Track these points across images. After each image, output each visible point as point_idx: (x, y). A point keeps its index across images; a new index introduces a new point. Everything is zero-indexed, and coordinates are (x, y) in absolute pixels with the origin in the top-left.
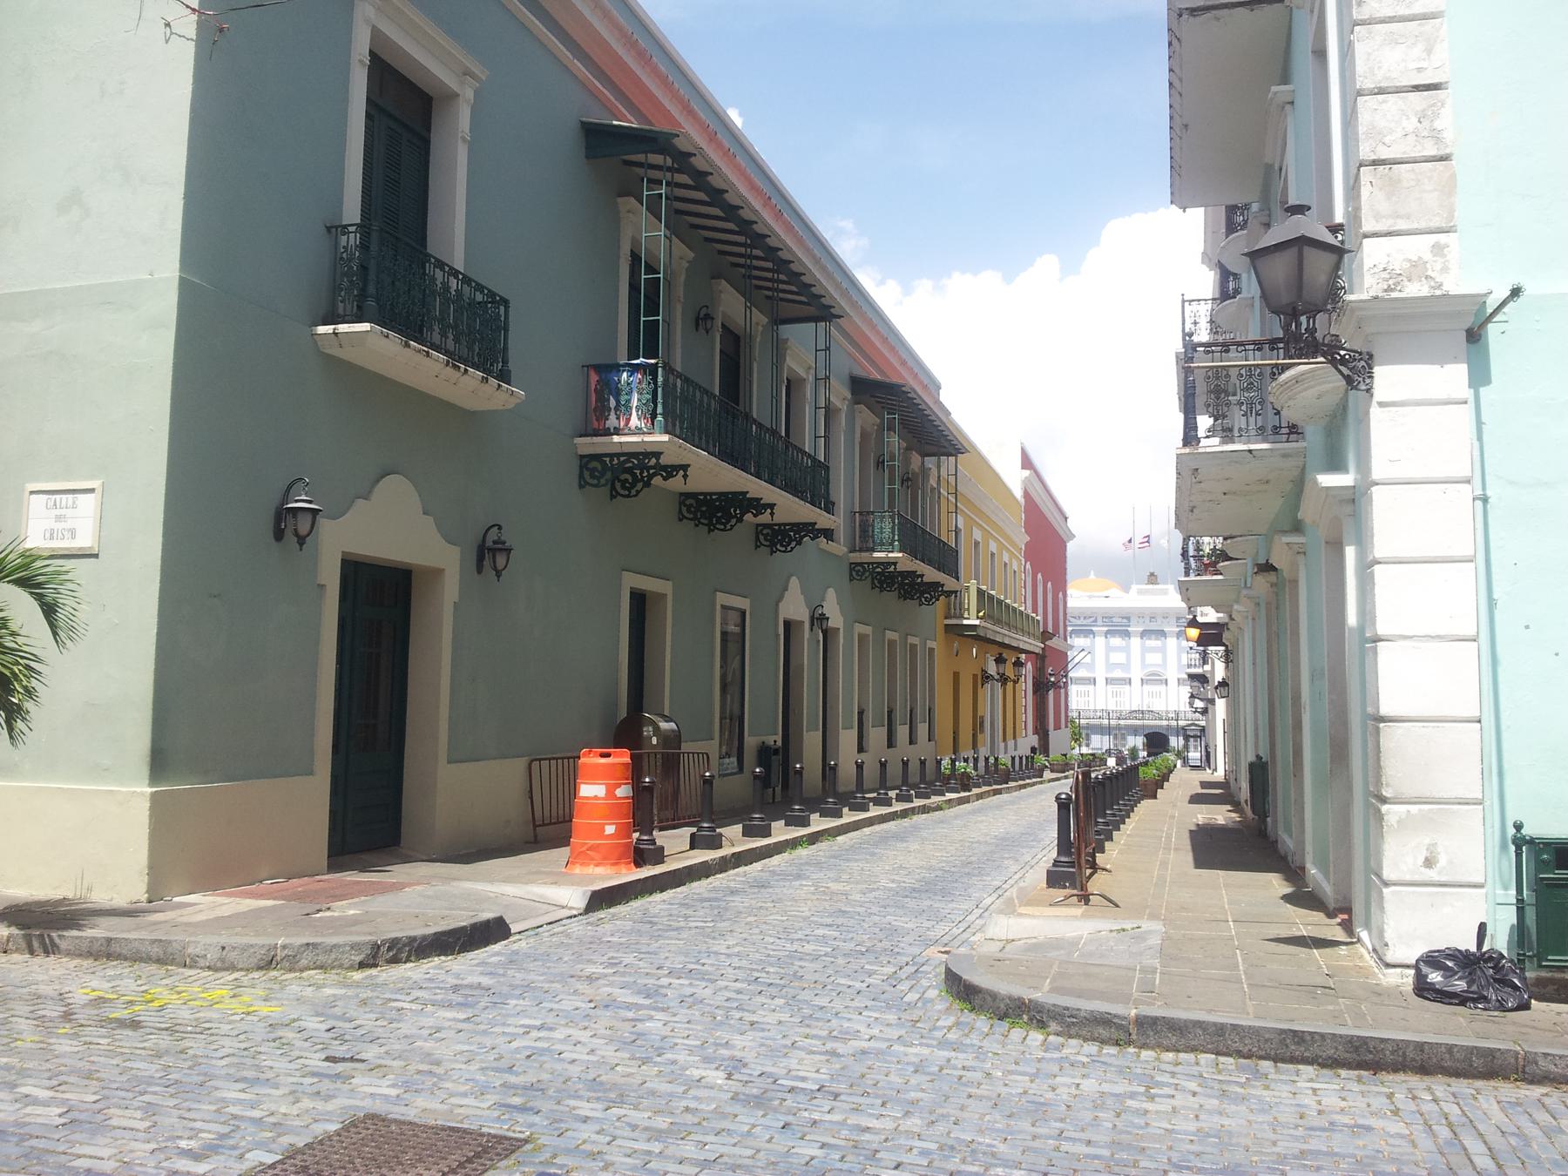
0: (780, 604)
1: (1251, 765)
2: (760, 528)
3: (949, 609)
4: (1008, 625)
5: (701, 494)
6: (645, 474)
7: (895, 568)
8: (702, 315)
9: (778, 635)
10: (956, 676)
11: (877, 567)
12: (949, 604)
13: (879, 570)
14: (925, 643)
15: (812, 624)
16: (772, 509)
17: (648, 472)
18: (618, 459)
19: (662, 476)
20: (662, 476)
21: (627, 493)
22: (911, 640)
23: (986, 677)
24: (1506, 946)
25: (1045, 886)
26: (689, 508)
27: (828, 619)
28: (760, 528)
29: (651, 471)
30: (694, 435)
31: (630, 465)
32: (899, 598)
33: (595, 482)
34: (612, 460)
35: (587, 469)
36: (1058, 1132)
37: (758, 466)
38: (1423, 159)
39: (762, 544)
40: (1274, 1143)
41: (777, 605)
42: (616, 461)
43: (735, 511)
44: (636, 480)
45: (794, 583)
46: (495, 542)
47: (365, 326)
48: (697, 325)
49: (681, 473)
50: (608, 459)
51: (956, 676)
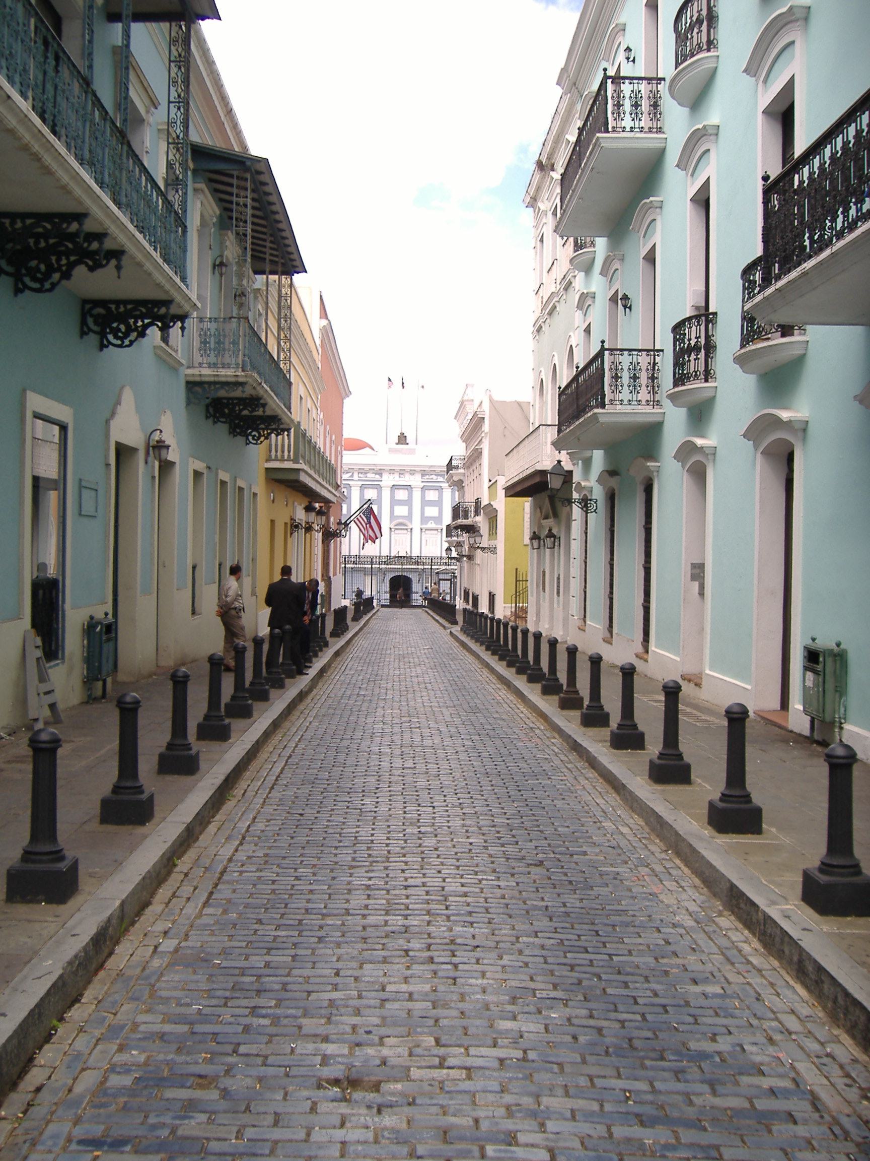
0: (111, 422)
2: (88, 306)
3: (270, 451)
4: (314, 467)
6: (64, 262)
7: (264, 411)
10: (272, 522)
12: (270, 445)
13: (245, 412)
14: (235, 481)
15: (147, 453)
16: (119, 260)
17: (68, 259)
18: (125, 307)
19: (87, 265)
20: (158, 326)
21: (119, 342)
22: (241, 483)
26: (96, 318)
27: (168, 447)
28: (88, 306)
29: (146, 321)
30: (84, 127)
31: (63, 248)
32: (207, 417)
33: (119, 342)
35: (91, 316)
38: (584, 535)
39: (90, 330)
41: (107, 422)
43: (59, 260)
44: (50, 270)
45: (128, 397)
46: (157, 442)
49: (179, 324)
50: (7, 222)
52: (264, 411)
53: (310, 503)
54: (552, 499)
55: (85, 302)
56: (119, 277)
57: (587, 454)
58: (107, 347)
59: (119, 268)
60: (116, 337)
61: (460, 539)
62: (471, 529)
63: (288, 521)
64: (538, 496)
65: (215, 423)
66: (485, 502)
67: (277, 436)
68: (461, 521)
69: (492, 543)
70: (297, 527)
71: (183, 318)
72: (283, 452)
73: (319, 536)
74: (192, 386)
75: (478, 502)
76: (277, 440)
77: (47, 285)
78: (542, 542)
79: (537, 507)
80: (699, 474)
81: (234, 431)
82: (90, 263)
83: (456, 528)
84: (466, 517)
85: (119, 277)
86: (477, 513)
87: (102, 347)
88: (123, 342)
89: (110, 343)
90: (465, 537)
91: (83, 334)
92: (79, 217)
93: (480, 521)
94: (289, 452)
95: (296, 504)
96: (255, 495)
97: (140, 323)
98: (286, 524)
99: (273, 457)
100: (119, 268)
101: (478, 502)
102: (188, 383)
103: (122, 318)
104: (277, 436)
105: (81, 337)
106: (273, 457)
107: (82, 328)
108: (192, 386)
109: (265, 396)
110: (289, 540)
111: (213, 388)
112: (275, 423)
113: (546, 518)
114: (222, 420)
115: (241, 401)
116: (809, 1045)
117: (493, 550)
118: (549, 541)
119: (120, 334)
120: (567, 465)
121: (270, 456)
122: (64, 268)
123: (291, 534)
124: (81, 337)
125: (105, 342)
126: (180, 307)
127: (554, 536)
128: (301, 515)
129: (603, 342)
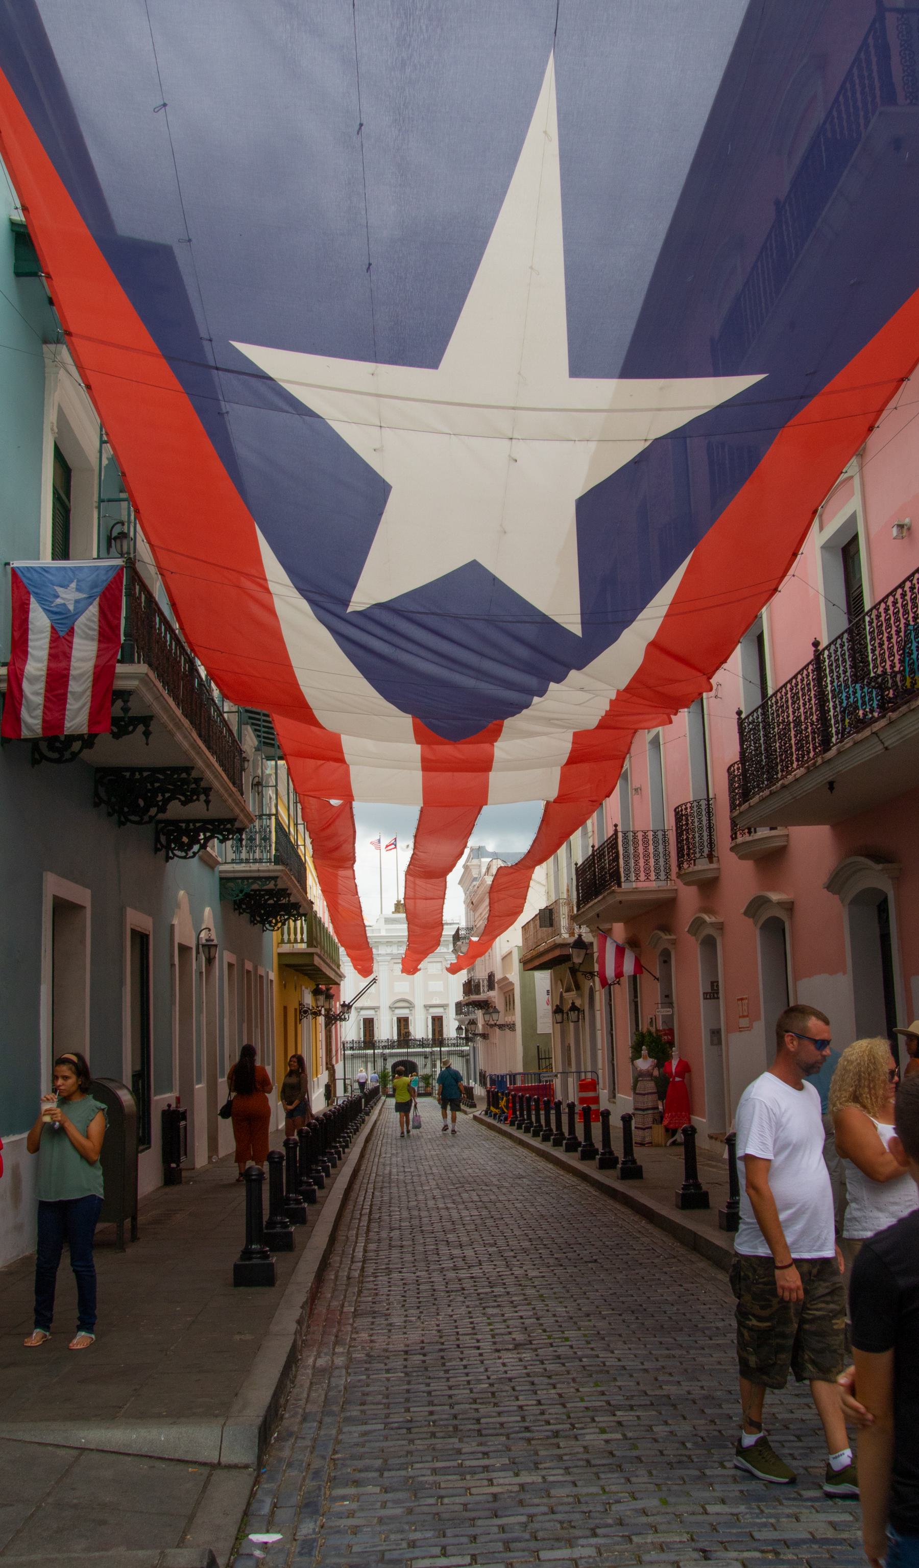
1: (164, 1112)
5: (127, 769)
7: (276, 885)
8: (114, 534)
9: (173, 965)
10: (285, 1008)
11: (253, 883)
13: (271, 902)
16: (147, 726)
17: (163, 796)
19: (180, 800)
20: (179, 799)
23: (303, 1012)
24: (578, 619)
25: (742, 911)
33: (55, 755)
34: (133, 774)
36: (419, 1495)
37: (56, 647)
39: (43, 757)
40: (506, 1372)
42: (137, 776)
46: (207, 940)
47: (274, 852)
48: (109, 546)
51: (285, 1008)
52: (276, 885)
53: (317, 985)
54: (574, 971)
55: (98, 770)
56: (147, 744)
57: (605, 926)
58: (172, 858)
59: (147, 734)
60: (181, 849)
61: (472, 1017)
62: (485, 1005)
63: (297, 1007)
64: (558, 967)
65: (121, 824)
66: (498, 976)
67: (295, 921)
68: (474, 997)
69: (509, 1019)
70: (306, 1012)
71: (240, 831)
72: (295, 934)
73: (321, 1020)
74: (225, 881)
75: (491, 976)
76: (295, 925)
77: (190, 854)
78: (565, 1015)
79: (556, 980)
80: (709, 944)
81: (240, 907)
82: (183, 798)
83: (468, 1004)
84: (478, 993)
85: (147, 744)
86: (491, 987)
87: (168, 859)
88: (142, 819)
89: (175, 855)
90: (479, 1015)
91: (157, 850)
92: (188, 770)
93: (494, 996)
94: (302, 934)
95: (303, 988)
96: (271, 981)
97: (160, 798)
98: (296, 1009)
99: (286, 941)
100: (147, 734)
101: (491, 976)
102: (221, 879)
103: (186, 832)
104: (295, 921)
105: (156, 853)
106: (286, 941)
107: (156, 845)
108: (225, 881)
109: (242, 816)
110: (299, 1026)
111: (246, 882)
112: (285, 898)
113: (568, 990)
114: (133, 818)
115: (270, 892)
116: (437, 1088)
117: (512, 1027)
118: (573, 1015)
119: (58, 744)
120: (588, 937)
121: (283, 940)
122: (160, 803)
123: (300, 1020)
124: (156, 853)
125: (171, 855)
126: (241, 822)
127: (578, 1009)
128: (308, 999)
129: (616, 826)
